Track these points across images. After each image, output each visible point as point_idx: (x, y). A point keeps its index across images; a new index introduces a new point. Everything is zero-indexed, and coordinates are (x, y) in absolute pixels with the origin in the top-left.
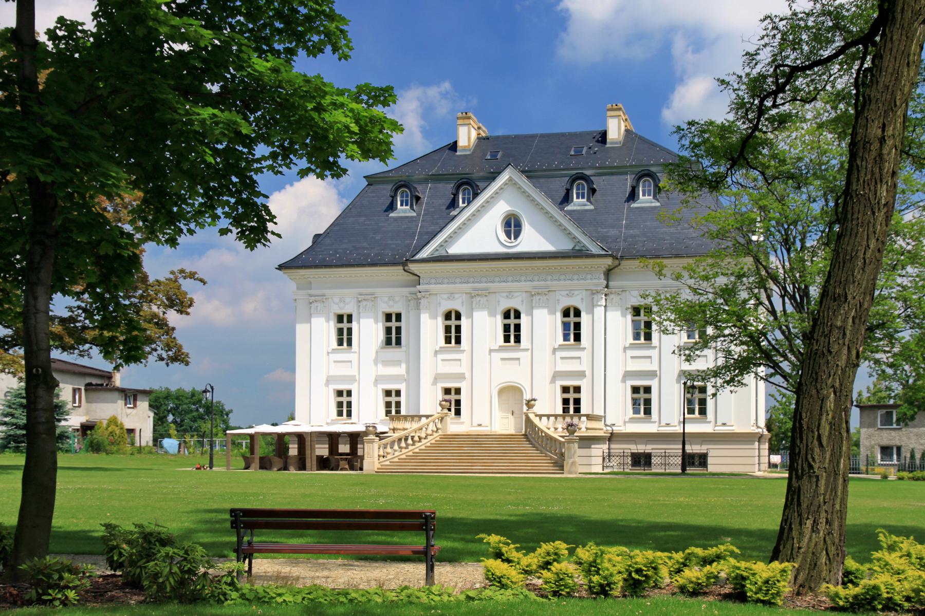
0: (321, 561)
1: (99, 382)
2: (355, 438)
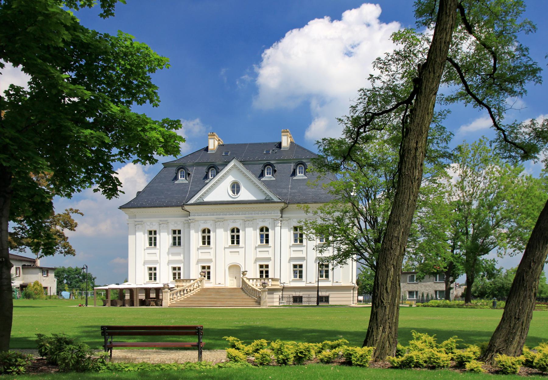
0: (145, 350)
1: (29, 264)
2: (158, 291)
